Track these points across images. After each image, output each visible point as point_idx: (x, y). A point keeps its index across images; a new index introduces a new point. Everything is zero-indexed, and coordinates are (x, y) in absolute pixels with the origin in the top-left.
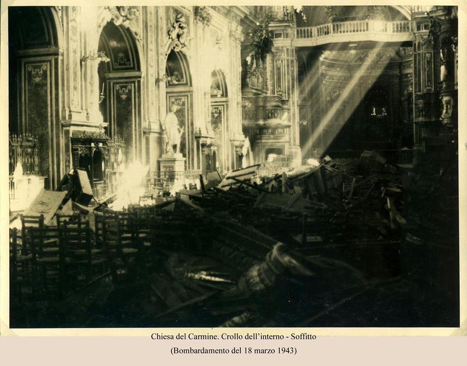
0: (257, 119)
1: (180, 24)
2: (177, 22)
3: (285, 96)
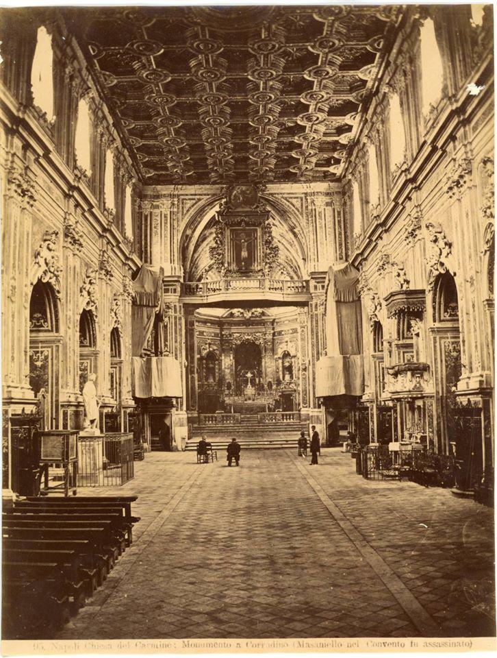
2: (88, 277)
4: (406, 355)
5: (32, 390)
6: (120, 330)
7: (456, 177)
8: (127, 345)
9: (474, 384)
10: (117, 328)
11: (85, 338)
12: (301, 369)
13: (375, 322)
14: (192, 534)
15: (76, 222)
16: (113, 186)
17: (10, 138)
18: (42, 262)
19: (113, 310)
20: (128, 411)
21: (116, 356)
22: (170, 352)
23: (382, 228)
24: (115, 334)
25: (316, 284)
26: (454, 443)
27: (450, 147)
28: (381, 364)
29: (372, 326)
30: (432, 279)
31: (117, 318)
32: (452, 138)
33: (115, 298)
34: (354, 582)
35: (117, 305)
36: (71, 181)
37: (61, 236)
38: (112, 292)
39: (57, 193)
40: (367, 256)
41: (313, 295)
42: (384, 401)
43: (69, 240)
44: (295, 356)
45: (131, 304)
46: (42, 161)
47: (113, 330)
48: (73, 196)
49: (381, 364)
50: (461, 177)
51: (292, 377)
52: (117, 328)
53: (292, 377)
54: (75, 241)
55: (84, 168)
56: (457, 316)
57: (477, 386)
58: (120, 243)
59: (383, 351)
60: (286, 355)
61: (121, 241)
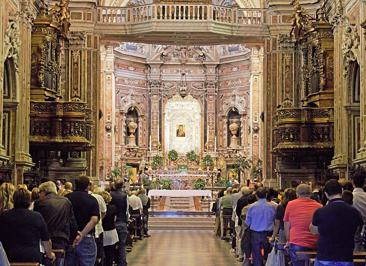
0: (53, 135)
3: (110, 142)
6: (15, 61)
8: (25, 82)
10: (12, 59)
12: (252, 130)
13: (351, 62)
14: (52, 159)
19: (7, 34)
20: (25, 169)
21: (8, 97)
22: (80, 98)
25: (275, 14)
28: (356, 118)
29: (346, 69)
31: (13, 44)
33: (11, 18)
34: (321, 39)
35: (12, 27)
38: (6, 9)
41: (271, 28)
42: (359, 164)
44: (245, 115)
45: (30, 31)
47: (6, 63)
49: (356, 118)
51: (240, 143)
52: (12, 59)
53: (240, 143)
59: (359, 102)
60: (234, 113)
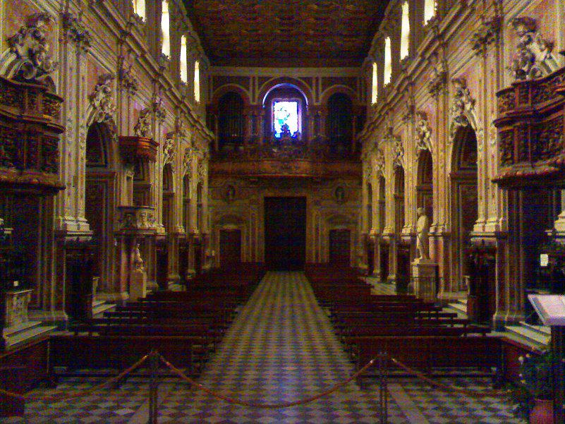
1: (35, 31)
4: (460, 186)
5: (87, 223)
7: (484, 35)
9: (408, 231)
10: (169, 165)
11: (139, 173)
13: (398, 167)
15: (130, 67)
16: (162, 23)
17: (119, 46)
18: (166, 152)
23: (440, 40)
24: (200, 186)
26: (469, 277)
27: (434, 59)
30: (455, 131)
32: (435, 53)
36: (123, 27)
37: (115, 82)
39: (109, 39)
40: (416, 80)
43: (123, 83)
46: (140, 60)
48: (158, 81)
50: (409, 114)
52: (169, 165)
54: (129, 85)
55: (140, 16)
56: (476, 165)
57: (494, 230)
58: (145, 53)
61: (146, 50)
